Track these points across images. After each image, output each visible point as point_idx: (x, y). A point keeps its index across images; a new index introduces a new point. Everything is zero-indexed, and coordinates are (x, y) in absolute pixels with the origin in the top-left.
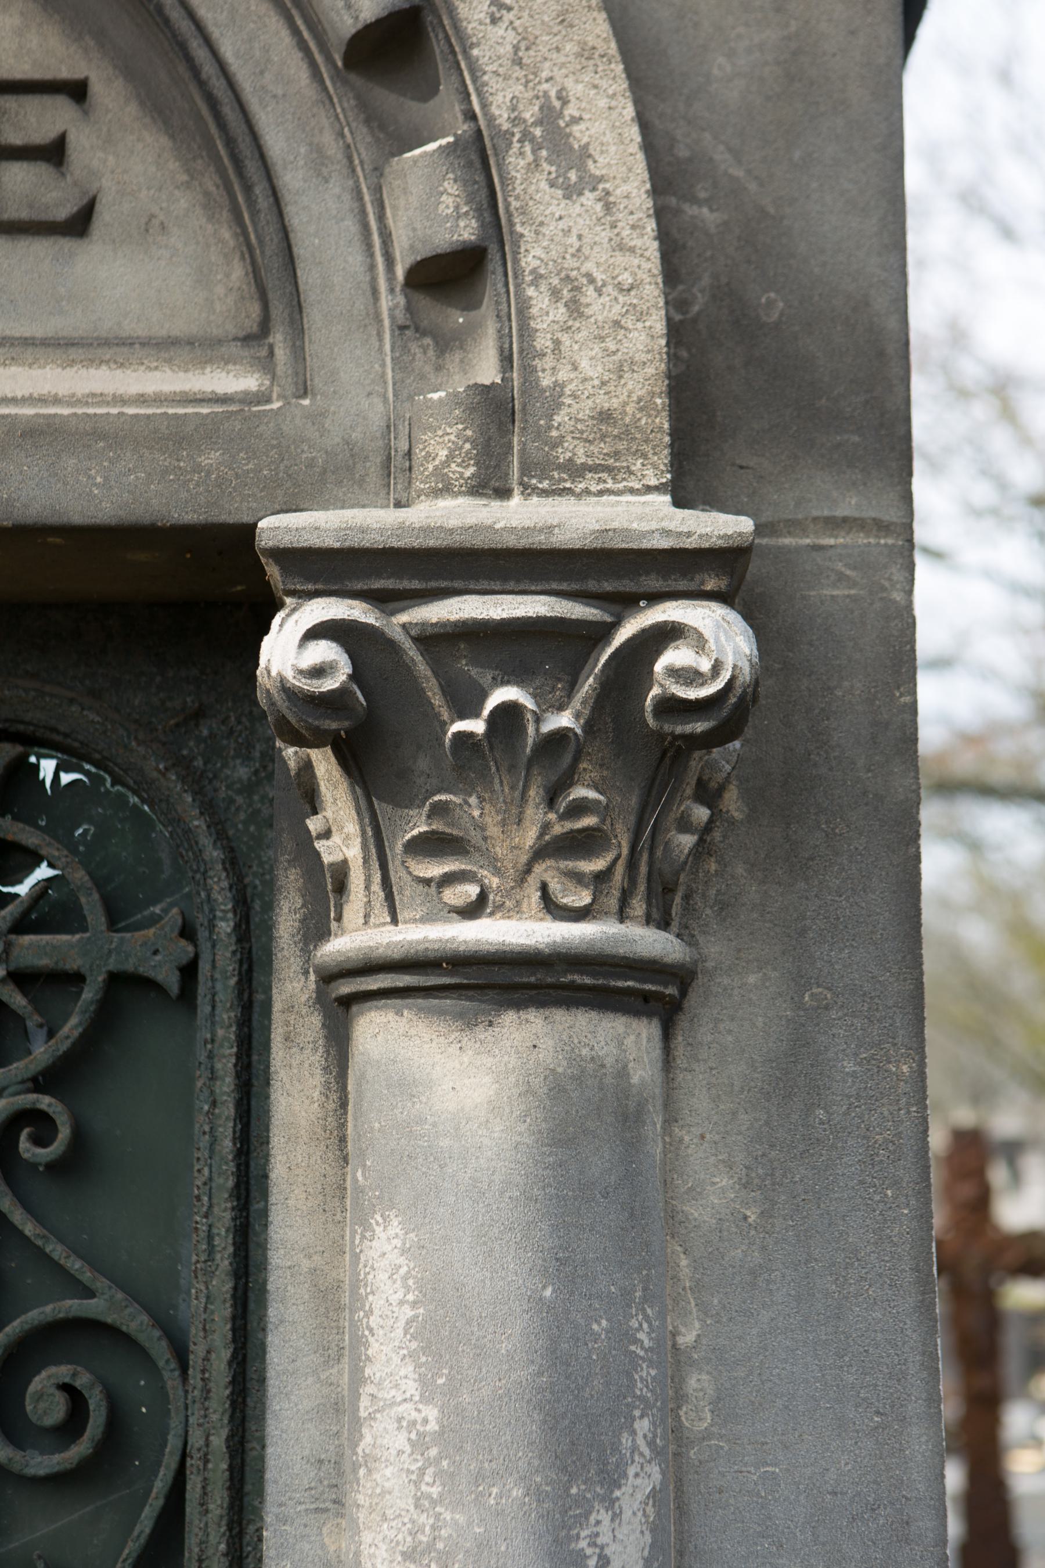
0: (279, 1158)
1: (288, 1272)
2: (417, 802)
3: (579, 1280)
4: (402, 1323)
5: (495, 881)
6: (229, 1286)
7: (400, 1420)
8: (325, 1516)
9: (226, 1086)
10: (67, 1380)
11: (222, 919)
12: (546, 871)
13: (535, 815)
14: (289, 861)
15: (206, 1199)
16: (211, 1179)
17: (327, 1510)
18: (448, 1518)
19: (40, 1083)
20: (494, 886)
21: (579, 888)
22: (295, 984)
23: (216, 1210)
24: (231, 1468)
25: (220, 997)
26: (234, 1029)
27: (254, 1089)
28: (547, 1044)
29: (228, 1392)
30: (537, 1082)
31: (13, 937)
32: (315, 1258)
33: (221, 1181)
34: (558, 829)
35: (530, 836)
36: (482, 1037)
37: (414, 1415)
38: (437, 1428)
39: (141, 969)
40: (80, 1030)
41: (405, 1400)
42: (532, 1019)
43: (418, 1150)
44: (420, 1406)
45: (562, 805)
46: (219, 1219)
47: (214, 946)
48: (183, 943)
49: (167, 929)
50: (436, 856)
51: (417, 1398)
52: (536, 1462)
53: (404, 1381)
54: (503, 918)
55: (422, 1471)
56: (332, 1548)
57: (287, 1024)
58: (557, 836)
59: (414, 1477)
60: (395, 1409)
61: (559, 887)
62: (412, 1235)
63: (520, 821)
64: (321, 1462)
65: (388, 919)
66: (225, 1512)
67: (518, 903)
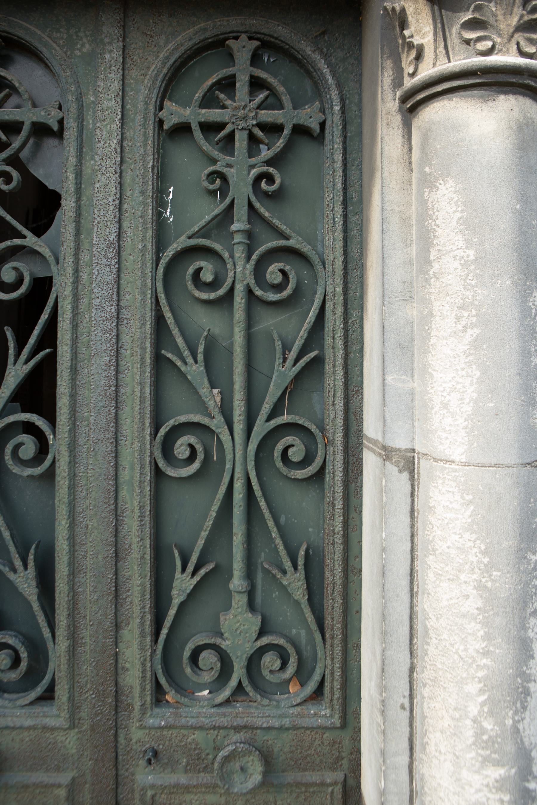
0: (386, 169)
1: (390, 212)
2: (464, 9)
3: (528, 203)
4: (455, 219)
5: (498, 40)
6: (342, 235)
7: (455, 257)
8: (407, 302)
9: (339, 165)
10: (282, 268)
11: (336, 105)
12: (519, 37)
13: (518, 11)
14: (387, 57)
15: (332, 205)
16: (333, 198)
17: (407, 300)
18: (480, 292)
19: (269, 162)
20: (499, 42)
21: (531, 46)
22: (390, 104)
23: (336, 209)
24: (344, 299)
25: (336, 133)
26: (341, 144)
27: (348, 167)
28: (516, 109)
29: (342, 272)
30: (513, 124)
31: (258, 110)
32: (401, 207)
33: (338, 198)
34: (526, 18)
35: (514, 21)
36: (491, 105)
37: (463, 254)
38: (474, 258)
39: (305, 123)
40: (283, 144)
41: (458, 249)
42: (511, 99)
43: (462, 152)
44: (466, 250)
45: (529, 8)
46: (337, 212)
47: (333, 115)
48: (321, 114)
49: (315, 109)
50: (473, 30)
51: (464, 247)
52: (515, 271)
53: (457, 242)
54: (501, 55)
55: (467, 275)
56: (410, 314)
57: (388, 118)
58: (525, 21)
59: (463, 278)
60: (452, 253)
61: (524, 44)
62: (460, 185)
63: (511, 13)
64: (405, 282)
65: (447, 61)
66: (342, 314)
67: (508, 50)
